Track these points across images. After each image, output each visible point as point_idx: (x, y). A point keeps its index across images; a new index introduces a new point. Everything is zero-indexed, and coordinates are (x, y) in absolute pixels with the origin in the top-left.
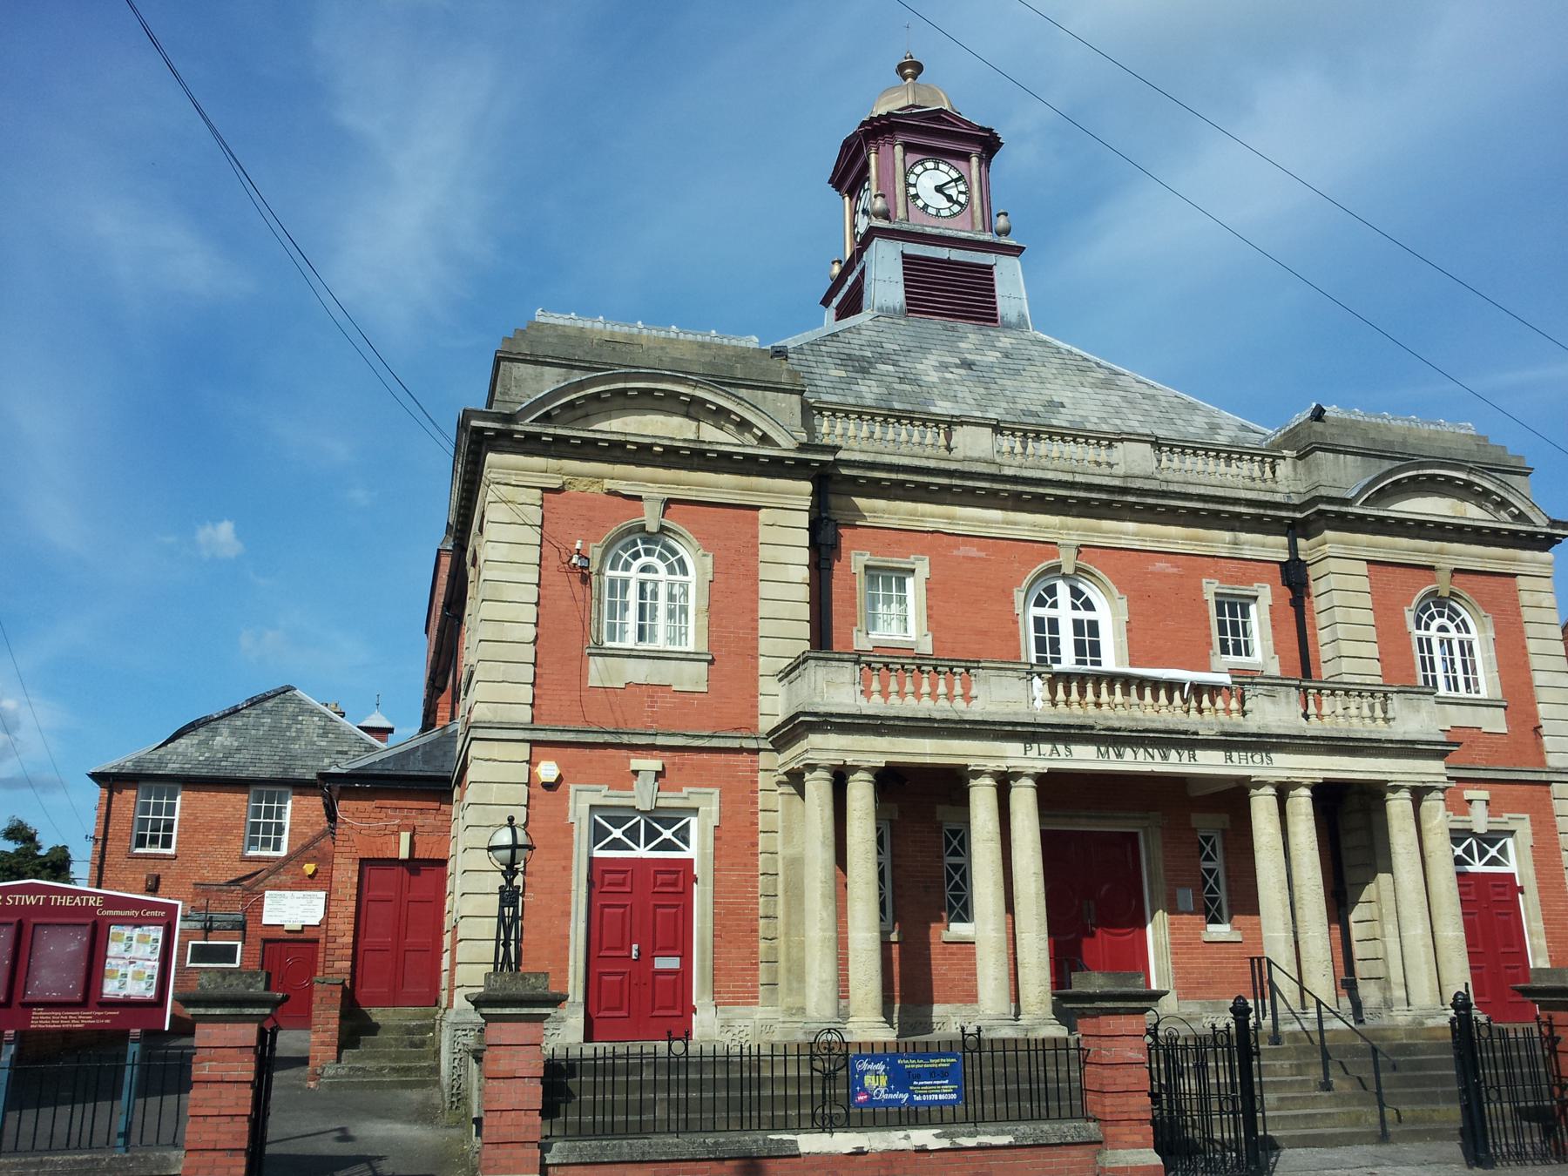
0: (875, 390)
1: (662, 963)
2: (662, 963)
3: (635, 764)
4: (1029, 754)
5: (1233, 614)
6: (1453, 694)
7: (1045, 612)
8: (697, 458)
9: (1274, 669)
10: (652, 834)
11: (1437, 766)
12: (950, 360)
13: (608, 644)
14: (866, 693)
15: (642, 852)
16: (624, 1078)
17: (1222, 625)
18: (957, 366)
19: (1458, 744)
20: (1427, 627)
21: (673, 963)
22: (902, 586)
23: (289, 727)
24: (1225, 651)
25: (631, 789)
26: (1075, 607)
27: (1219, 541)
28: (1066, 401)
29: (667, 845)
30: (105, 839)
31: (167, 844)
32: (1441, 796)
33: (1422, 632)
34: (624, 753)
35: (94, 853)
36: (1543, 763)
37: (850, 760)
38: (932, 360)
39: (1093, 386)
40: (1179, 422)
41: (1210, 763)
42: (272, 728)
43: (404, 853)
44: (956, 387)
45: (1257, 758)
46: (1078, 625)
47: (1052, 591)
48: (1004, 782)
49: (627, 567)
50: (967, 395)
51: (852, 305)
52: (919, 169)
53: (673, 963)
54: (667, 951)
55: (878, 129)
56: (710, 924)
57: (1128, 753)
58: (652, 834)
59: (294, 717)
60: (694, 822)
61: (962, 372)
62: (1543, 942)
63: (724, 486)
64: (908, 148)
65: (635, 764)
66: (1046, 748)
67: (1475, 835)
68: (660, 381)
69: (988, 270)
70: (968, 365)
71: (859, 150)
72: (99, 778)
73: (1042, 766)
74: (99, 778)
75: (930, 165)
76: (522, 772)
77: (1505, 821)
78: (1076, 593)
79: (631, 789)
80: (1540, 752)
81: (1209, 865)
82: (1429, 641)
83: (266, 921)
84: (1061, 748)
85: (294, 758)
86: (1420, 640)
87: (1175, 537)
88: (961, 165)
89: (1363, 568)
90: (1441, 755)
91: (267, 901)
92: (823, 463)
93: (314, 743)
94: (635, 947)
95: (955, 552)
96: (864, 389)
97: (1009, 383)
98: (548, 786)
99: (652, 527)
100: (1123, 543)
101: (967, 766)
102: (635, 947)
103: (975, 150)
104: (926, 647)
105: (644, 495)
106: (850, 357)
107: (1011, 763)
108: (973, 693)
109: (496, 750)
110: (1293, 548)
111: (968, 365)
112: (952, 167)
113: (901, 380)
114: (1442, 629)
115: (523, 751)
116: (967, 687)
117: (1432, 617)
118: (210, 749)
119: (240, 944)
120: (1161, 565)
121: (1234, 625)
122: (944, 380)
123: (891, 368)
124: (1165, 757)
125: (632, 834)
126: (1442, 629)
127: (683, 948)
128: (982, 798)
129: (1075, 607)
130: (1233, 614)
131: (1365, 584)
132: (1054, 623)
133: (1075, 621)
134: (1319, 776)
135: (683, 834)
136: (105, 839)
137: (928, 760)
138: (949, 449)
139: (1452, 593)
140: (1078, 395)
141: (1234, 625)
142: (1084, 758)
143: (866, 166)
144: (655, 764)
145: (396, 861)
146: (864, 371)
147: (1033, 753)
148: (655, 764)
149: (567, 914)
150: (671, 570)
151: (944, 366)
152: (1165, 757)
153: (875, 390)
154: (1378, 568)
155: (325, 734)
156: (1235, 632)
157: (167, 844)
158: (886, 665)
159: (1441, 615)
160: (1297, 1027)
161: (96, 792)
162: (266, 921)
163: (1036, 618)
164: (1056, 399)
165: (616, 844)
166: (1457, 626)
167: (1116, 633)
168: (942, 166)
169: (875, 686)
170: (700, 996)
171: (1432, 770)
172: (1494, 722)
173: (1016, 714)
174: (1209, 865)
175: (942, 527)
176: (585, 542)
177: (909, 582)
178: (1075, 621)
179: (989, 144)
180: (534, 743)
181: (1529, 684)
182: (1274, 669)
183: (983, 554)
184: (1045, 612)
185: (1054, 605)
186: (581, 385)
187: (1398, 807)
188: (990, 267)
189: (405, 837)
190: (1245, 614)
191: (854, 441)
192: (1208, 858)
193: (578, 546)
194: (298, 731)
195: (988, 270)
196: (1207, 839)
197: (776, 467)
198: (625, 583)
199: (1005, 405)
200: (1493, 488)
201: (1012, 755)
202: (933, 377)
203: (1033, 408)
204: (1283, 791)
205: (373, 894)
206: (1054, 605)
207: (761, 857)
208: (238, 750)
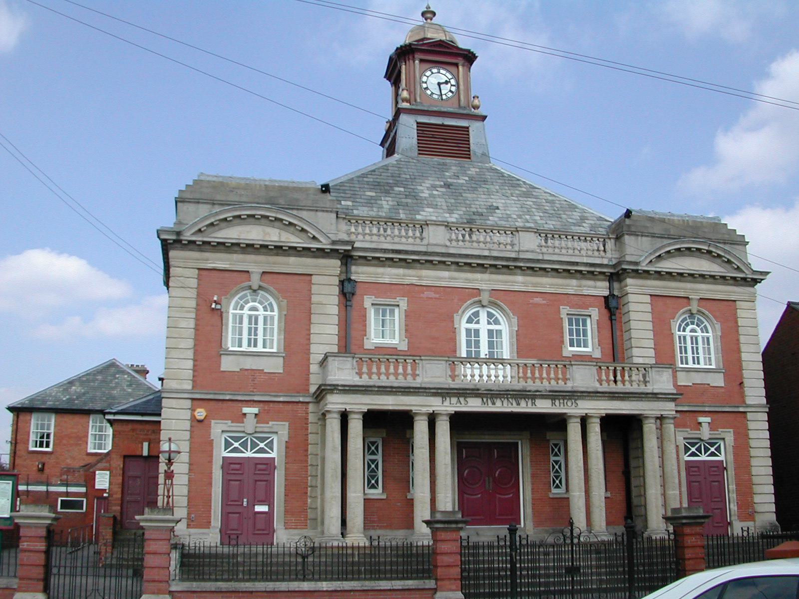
0: (390, 203)
1: (259, 508)
2: (259, 508)
3: (246, 410)
4: (445, 404)
5: (577, 324)
6: (696, 366)
7: (472, 326)
8: (279, 250)
9: (597, 354)
10: (254, 445)
11: (671, 406)
12: (438, 183)
13: (231, 349)
14: (360, 374)
15: (249, 454)
16: (255, 568)
17: (571, 331)
18: (441, 187)
19: (682, 394)
20: (684, 331)
21: (264, 508)
22: (392, 313)
23: (111, 381)
24: (572, 345)
25: (243, 423)
26: (489, 323)
27: (571, 286)
28: (500, 205)
29: (262, 451)
30: (16, 443)
31: (47, 446)
32: (672, 421)
33: (681, 333)
34: (240, 404)
35: (11, 450)
36: (744, 402)
37: (348, 408)
38: (428, 183)
39: (519, 196)
40: (564, 216)
41: (543, 407)
42: (103, 381)
43: (145, 453)
44: (438, 199)
45: (569, 403)
46: (490, 332)
47: (476, 314)
48: (432, 420)
49: (242, 308)
50: (444, 204)
51: (390, 152)
52: (428, 73)
53: (264, 508)
54: (262, 502)
55: (404, 53)
56: (283, 490)
57: (498, 403)
58: (254, 445)
59: (114, 376)
60: (275, 438)
61: (443, 190)
62: (735, 495)
63: (293, 264)
64: (421, 61)
65: (246, 410)
66: (454, 400)
67: (702, 440)
68: (259, 210)
69: (467, 129)
70: (448, 186)
71: (396, 65)
72: (11, 409)
73: (452, 410)
74: (11, 409)
75: (435, 70)
76: (187, 415)
77: (722, 432)
78: (490, 315)
79: (243, 423)
80: (742, 395)
81: (556, 458)
82: (685, 337)
83: (97, 487)
84: (462, 399)
85: (114, 398)
86: (680, 337)
87: (548, 284)
88: (453, 69)
89: (648, 299)
90: (674, 400)
91: (97, 476)
92: (345, 250)
93: (124, 390)
94: (245, 500)
95: (422, 295)
96: (384, 203)
97: (469, 195)
98: (200, 421)
99: (255, 287)
100: (516, 288)
101: (411, 411)
102: (245, 500)
103: (460, 61)
104: (404, 347)
105: (250, 270)
106: (379, 184)
107: (434, 409)
108: (417, 372)
109: (173, 403)
110: (610, 288)
111: (448, 186)
112: (448, 71)
113: (406, 197)
114: (693, 331)
115: (188, 403)
116: (414, 369)
117: (687, 325)
118: (69, 394)
119: (85, 500)
120: (538, 300)
121: (578, 331)
122: (431, 195)
123: (402, 189)
124: (518, 404)
125: (244, 445)
126: (693, 331)
127: (268, 499)
128: (421, 428)
129: (489, 323)
130: (577, 324)
131: (648, 308)
132: (477, 332)
133: (489, 330)
134: (603, 413)
135: (270, 445)
136: (16, 443)
137: (391, 408)
138: (422, 239)
139: (699, 311)
140: (508, 201)
141: (578, 331)
142: (474, 405)
143: (400, 72)
144: (255, 410)
145: (141, 456)
146: (387, 192)
147: (447, 403)
148: (255, 410)
149: (210, 484)
150: (265, 309)
151: (434, 187)
152: (518, 404)
153: (390, 203)
154: (657, 298)
155: (130, 385)
156: (578, 335)
157: (47, 446)
158: (370, 359)
159: (693, 323)
160: (596, 540)
161: (10, 416)
162: (97, 487)
163: (467, 329)
164: (495, 204)
165: (236, 450)
166: (701, 329)
167: (511, 337)
168: (442, 71)
169: (365, 369)
170: (278, 523)
171: (668, 409)
172: (718, 381)
173: (439, 383)
174: (556, 458)
175: (414, 282)
176: (219, 297)
177: (397, 310)
178: (489, 330)
179: (469, 58)
180: (193, 399)
181: (739, 360)
182: (597, 354)
183: (437, 296)
184: (472, 326)
185: (478, 322)
186: (217, 214)
187: (650, 429)
188: (468, 128)
189: (146, 445)
190: (584, 324)
191: (365, 239)
192: (556, 455)
193: (215, 299)
194: (117, 383)
195: (467, 129)
196: (556, 445)
197: (321, 253)
198: (241, 317)
199: (464, 209)
200: (723, 254)
201: (436, 404)
202: (426, 194)
203: (480, 210)
204: (584, 421)
205: (131, 473)
206: (478, 322)
207: (309, 457)
208: (84, 394)
